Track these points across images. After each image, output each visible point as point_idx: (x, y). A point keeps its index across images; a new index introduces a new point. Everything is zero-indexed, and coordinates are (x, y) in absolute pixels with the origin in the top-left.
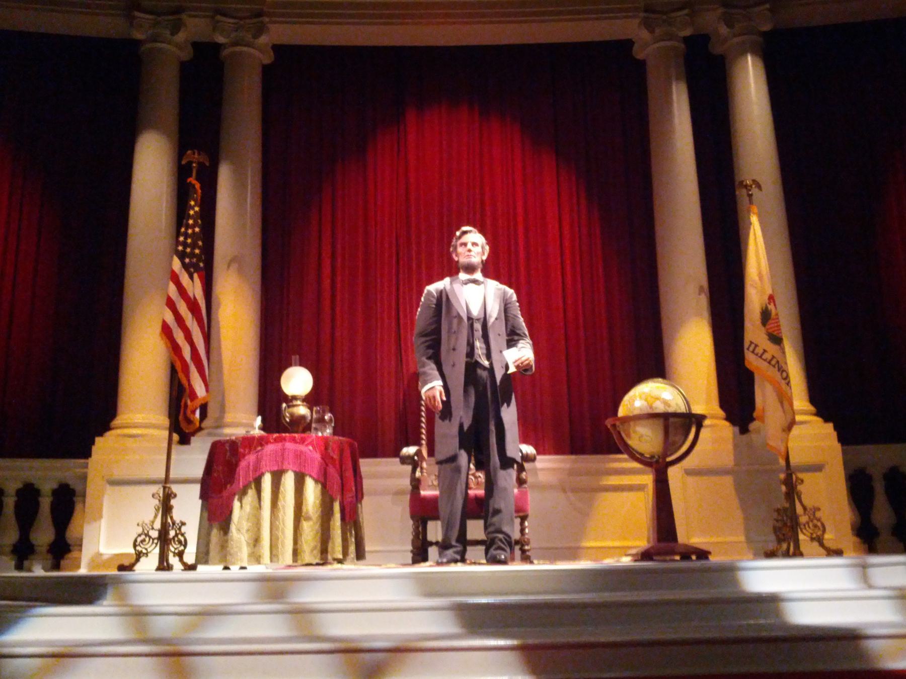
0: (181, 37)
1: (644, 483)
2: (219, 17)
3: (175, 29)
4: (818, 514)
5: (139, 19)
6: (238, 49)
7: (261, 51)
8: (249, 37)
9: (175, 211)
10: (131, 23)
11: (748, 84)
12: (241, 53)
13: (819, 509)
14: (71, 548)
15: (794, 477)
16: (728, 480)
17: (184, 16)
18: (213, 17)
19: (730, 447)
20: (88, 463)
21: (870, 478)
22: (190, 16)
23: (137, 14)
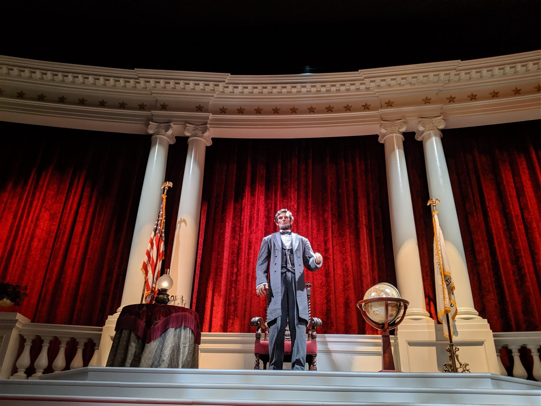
0: (170, 132)
1: (306, 346)
2: (187, 125)
3: (167, 130)
4: (468, 368)
5: (188, 127)
6: (195, 138)
7: (206, 139)
8: (200, 133)
9: (391, 223)
10: (185, 129)
11: (397, 167)
12: (200, 140)
13: (468, 365)
14: (36, 371)
15: (454, 348)
16: (434, 348)
17: (172, 124)
18: (184, 125)
19: (434, 330)
20: (102, 329)
21: (529, 351)
22: (174, 124)
23: (151, 123)
